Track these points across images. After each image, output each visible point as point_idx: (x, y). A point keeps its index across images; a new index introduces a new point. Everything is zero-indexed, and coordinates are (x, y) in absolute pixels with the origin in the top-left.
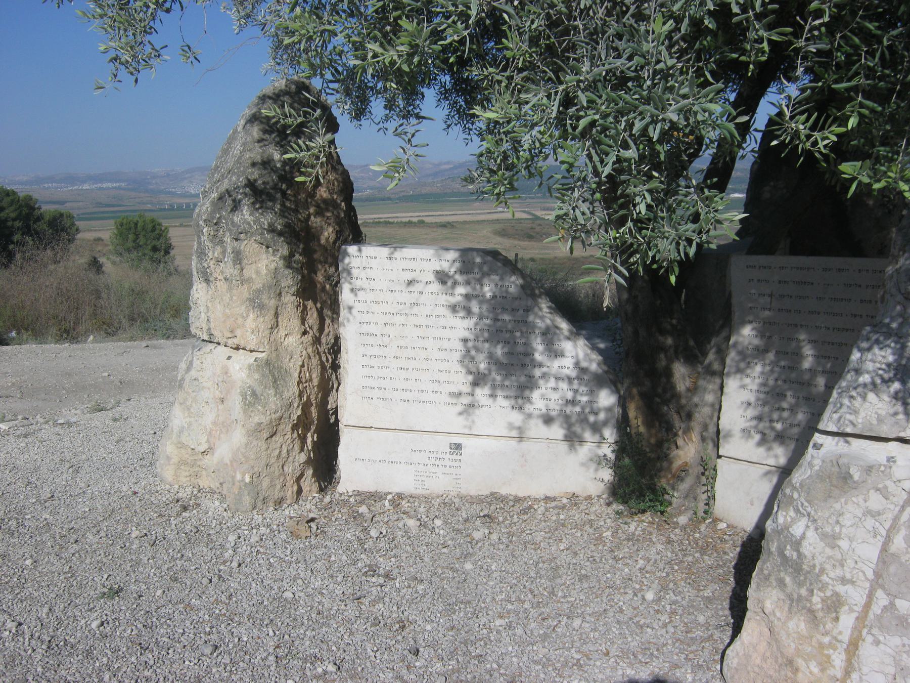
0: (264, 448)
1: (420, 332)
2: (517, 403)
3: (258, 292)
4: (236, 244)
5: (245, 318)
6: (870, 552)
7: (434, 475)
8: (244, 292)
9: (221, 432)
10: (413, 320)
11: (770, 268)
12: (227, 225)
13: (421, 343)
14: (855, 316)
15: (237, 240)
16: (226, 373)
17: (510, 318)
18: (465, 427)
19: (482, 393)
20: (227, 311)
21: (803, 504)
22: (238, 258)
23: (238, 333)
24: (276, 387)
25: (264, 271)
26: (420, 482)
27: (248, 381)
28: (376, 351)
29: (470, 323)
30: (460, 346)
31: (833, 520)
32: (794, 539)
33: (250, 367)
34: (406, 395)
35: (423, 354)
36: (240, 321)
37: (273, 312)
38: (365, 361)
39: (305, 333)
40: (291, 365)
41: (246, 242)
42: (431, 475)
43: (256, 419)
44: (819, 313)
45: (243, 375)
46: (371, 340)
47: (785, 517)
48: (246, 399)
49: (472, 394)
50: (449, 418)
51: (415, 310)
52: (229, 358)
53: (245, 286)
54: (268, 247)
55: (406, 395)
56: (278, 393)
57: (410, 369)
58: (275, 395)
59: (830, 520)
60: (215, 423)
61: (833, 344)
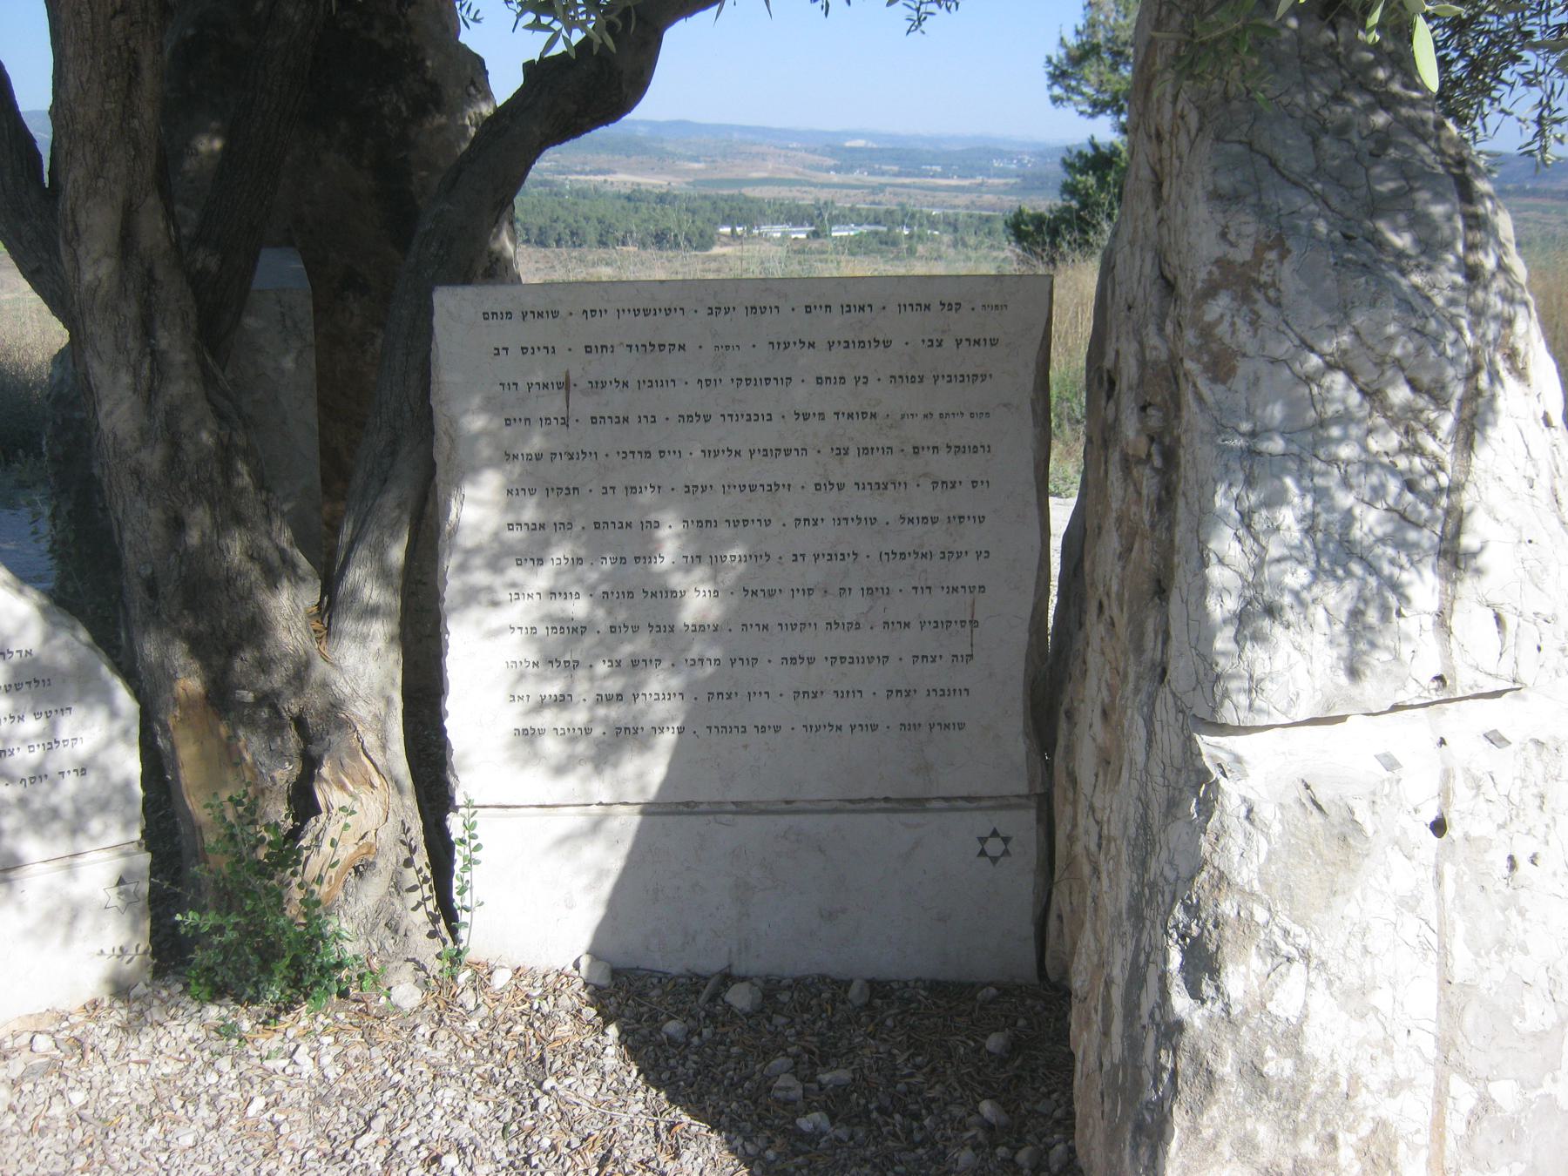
6: (1423, 999)
11: (555, 314)
14: (806, 417)
21: (1286, 933)
31: (1354, 952)
32: (1279, 1028)
44: (707, 418)
47: (1246, 977)
59: (1349, 952)
61: (753, 488)
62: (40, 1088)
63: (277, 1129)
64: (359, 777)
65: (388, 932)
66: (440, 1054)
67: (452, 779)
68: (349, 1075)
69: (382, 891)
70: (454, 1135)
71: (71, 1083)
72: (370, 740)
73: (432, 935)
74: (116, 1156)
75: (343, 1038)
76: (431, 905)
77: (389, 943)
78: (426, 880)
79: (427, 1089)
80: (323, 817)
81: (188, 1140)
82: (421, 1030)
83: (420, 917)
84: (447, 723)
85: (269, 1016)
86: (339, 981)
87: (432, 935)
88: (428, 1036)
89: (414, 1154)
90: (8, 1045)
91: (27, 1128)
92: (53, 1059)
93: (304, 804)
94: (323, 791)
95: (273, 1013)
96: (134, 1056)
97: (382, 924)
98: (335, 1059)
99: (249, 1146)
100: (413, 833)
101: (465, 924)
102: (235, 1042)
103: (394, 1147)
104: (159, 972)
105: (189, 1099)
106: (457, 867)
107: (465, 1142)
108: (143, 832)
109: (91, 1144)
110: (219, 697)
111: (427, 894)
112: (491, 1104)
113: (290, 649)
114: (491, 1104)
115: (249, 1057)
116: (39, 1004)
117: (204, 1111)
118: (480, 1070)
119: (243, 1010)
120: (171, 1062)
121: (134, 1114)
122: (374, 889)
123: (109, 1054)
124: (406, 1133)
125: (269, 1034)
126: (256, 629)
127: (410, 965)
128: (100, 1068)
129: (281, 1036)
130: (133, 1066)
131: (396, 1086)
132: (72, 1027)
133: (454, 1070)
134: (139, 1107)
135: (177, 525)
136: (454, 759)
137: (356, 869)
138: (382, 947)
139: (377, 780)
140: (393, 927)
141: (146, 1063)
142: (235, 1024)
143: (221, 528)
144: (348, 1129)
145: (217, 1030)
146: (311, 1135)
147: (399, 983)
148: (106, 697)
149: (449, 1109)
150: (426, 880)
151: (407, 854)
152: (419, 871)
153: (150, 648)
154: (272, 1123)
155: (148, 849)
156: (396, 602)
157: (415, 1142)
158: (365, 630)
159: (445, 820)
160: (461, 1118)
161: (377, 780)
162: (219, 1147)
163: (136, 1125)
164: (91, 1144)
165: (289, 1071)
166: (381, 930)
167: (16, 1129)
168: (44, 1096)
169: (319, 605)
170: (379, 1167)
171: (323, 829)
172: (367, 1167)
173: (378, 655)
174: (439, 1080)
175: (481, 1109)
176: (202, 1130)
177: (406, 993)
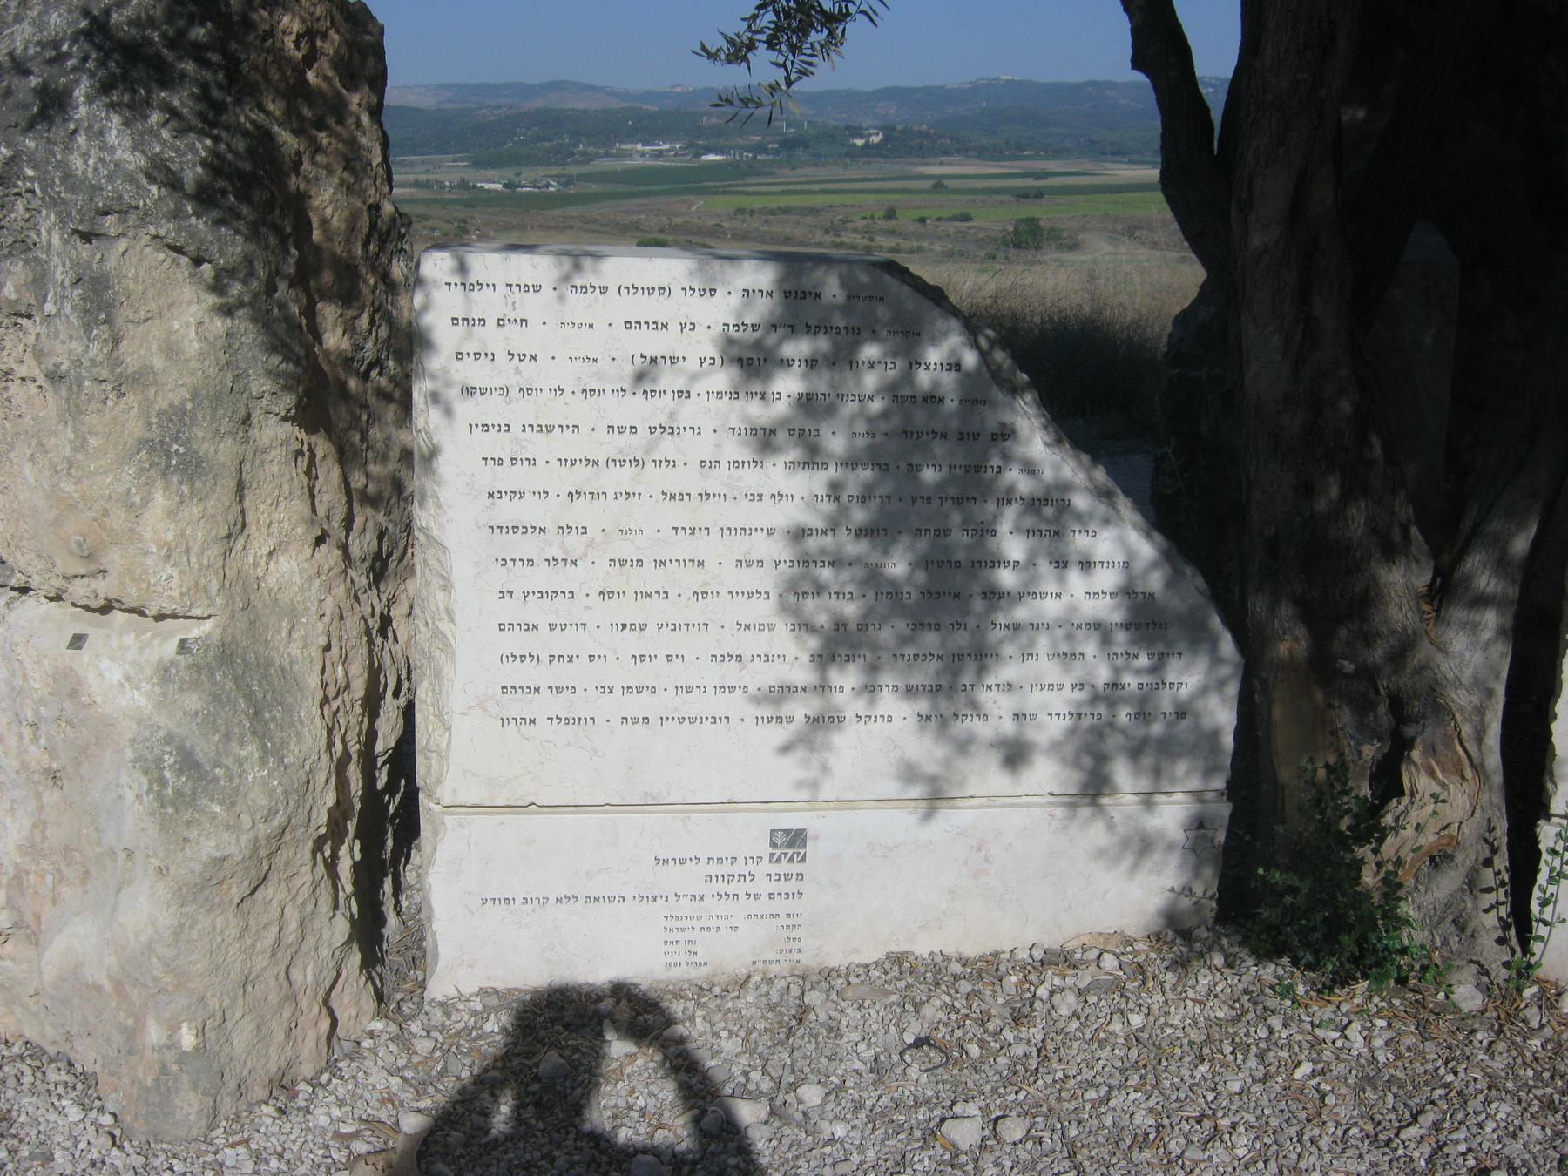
0: (234, 932)
1: (679, 514)
2: (935, 706)
3: (178, 417)
4: (84, 251)
5: (136, 512)
7: (723, 923)
8: (130, 418)
9: (61, 879)
10: (659, 480)
12: (47, 185)
13: (685, 547)
15: (87, 237)
16: (74, 694)
17: (294, 177)
18: (800, 784)
19: (847, 678)
20: (68, 487)
22: (99, 301)
23: (114, 559)
24: (262, 735)
25: (193, 346)
26: (682, 947)
27: (162, 720)
28: (541, 578)
29: (815, 482)
30: (777, 550)
33: (164, 672)
34: (638, 705)
35: (690, 579)
36: (118, 520)
37: (233, 484)
38: (511, 610)
39: (320, 541)
40: (295, 650)
41: (122, 244)
42: (714, 923)
43: (209, 848)
45: (141, 699)
46: (526, 546)
48: (162, 782)
49: (823, 687)
50: (748, 760)
51: (667, 447)
52: (78, 641)
53: (131, 398)
54: (198, 262)
55: (638, 705)
56: (272, 752)
57: (652, 628)
58: (263, 761)
60: (31, 849)
62: (1103, 1003)
63: (1322, 1099)
64: (1450, 766)
65: (1453, 929)
66: (1498, 1064)
67: (1549, 785)
68: (1399, 1063)
69: (1455, 886)
70: (1506, 1151)
71: (1131, 1005)
72: (1467, 730)
73: (1501, 941)
74: (1167, 1083)
75: (1397, 1024)
76: (1504, 911)
77: (1454, 940)
78: (1503, 884)
79: (1481, 1098)
80: (1406, 800)
81: (1236, 1087)
82: (1479, 1036)
83: (1491, 920)
84: (1554, 726)
85: (1324, 986)
86: (1399, 967)
87: (1501, 941)
88: (1485, 1043)
89: (1461, 1160)
90: (1078, 956)
91: (1088, 1036)
92: (1118, 978)
93: (1389, 782)
94: (1410, 774)
95: (1328, 983)
96: (1191, 994)
97: (1450, 919)
98: (1387, 1043)
99: (1294, 1107)
100: (1498, 832)
101: (1541, 938)
102: (1288, 1003)
103: (1440, 1148)
104: (1222, 917)
105: (1240, 1047)
106: (1542, 878)
107: (1518, 1163)
108: (1228, 783)
109: (1145, 1066)
110: (1321, 667)
111: (1502, 898)
112: (1548, 1131)
113: (1399, 627)
114: (1548, 1131)
115: (1301, 1021)
116: (1110, 923)
117: (1252, 1062)
118: (1539, 1093)
119: (1298, 974)
120: (1225, 1008)
121: (1186, 1048)
122: (1447, 883)
123: (1168, 986)
124: (1454, 1136)
125: (1323, 1003)
126: (1366, 601)
127: (1474, 968)
128: (1158, 997)
129: (1334, 1008)
130: (1189, 1003)
131: (1448, 1086)
132: (1136, 953)
133: (1510, 1085)
134: (1191, 1043)
135: (1308, 490)
136: (1555, 765)
137: (1432, 859)
138: (1445, 943)
139: (1469, 773)
140: (1460, 925)
141: (1201, 1003)
142: (1291, 986)
143: (1347, 496)
144: (1393, 1116)
145: (1272, 988)
146: (1355, 1113)
147: (1460, 983)
148: (1214, 642)
149: (1503, 1124)
150: (1503, 884)
151: (1488, 853)
152: (1498, 873)
153: (1258, 605)
154: (1318, 1091)
155: (1229, 799)
156: (1514, 592)
157: (1462, 1148)
158: (1477, 618)
159: (1535, 826)
160: (1514, 1136)
161: (1469, 773)
162: (1265, 1101)
163: (1187, 1059)
164: (1145, 1066)
165: (1339, 1044)
166: (1447, 925)
167: (1079, 1034)
168: (1106, 1011)
169: (1430, 586)
170: (1423, 1163)
171: (1406, 812)
172: (1411, 1160)
173: (1486, 647)
174: (1494, 1092)
175: (1537, 1132)
176: (1249, 1081)
177: (1467, 996)
